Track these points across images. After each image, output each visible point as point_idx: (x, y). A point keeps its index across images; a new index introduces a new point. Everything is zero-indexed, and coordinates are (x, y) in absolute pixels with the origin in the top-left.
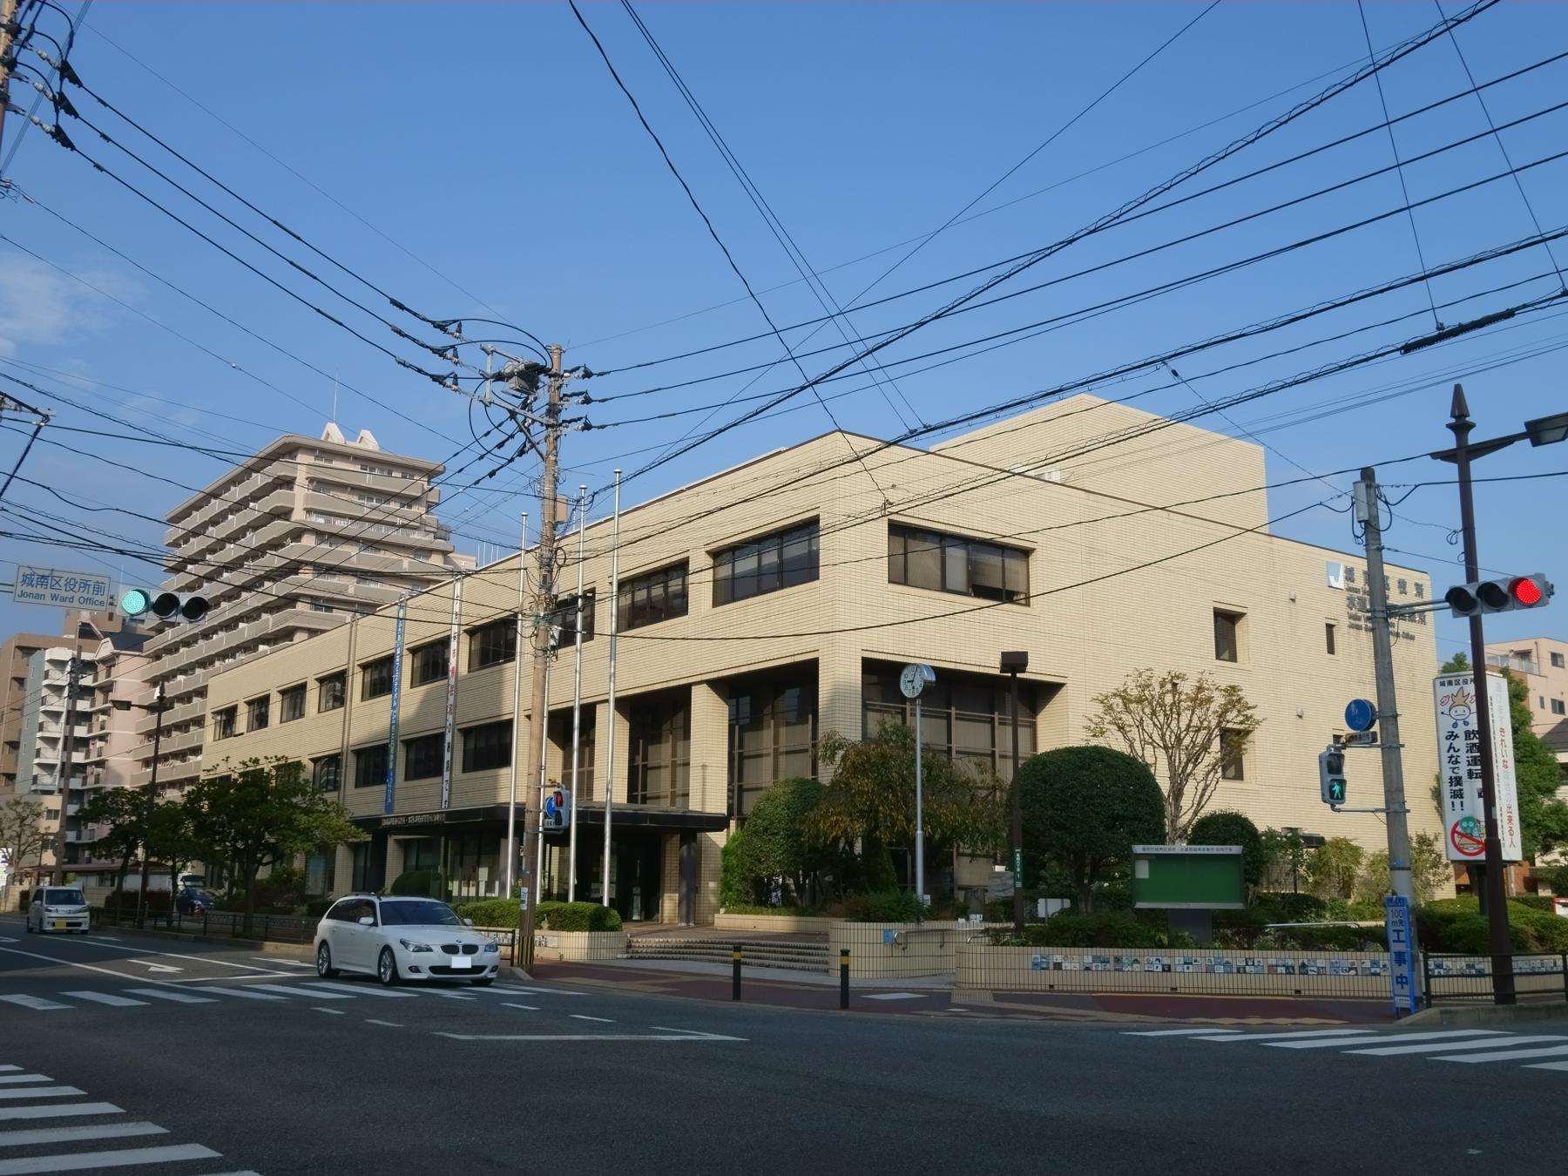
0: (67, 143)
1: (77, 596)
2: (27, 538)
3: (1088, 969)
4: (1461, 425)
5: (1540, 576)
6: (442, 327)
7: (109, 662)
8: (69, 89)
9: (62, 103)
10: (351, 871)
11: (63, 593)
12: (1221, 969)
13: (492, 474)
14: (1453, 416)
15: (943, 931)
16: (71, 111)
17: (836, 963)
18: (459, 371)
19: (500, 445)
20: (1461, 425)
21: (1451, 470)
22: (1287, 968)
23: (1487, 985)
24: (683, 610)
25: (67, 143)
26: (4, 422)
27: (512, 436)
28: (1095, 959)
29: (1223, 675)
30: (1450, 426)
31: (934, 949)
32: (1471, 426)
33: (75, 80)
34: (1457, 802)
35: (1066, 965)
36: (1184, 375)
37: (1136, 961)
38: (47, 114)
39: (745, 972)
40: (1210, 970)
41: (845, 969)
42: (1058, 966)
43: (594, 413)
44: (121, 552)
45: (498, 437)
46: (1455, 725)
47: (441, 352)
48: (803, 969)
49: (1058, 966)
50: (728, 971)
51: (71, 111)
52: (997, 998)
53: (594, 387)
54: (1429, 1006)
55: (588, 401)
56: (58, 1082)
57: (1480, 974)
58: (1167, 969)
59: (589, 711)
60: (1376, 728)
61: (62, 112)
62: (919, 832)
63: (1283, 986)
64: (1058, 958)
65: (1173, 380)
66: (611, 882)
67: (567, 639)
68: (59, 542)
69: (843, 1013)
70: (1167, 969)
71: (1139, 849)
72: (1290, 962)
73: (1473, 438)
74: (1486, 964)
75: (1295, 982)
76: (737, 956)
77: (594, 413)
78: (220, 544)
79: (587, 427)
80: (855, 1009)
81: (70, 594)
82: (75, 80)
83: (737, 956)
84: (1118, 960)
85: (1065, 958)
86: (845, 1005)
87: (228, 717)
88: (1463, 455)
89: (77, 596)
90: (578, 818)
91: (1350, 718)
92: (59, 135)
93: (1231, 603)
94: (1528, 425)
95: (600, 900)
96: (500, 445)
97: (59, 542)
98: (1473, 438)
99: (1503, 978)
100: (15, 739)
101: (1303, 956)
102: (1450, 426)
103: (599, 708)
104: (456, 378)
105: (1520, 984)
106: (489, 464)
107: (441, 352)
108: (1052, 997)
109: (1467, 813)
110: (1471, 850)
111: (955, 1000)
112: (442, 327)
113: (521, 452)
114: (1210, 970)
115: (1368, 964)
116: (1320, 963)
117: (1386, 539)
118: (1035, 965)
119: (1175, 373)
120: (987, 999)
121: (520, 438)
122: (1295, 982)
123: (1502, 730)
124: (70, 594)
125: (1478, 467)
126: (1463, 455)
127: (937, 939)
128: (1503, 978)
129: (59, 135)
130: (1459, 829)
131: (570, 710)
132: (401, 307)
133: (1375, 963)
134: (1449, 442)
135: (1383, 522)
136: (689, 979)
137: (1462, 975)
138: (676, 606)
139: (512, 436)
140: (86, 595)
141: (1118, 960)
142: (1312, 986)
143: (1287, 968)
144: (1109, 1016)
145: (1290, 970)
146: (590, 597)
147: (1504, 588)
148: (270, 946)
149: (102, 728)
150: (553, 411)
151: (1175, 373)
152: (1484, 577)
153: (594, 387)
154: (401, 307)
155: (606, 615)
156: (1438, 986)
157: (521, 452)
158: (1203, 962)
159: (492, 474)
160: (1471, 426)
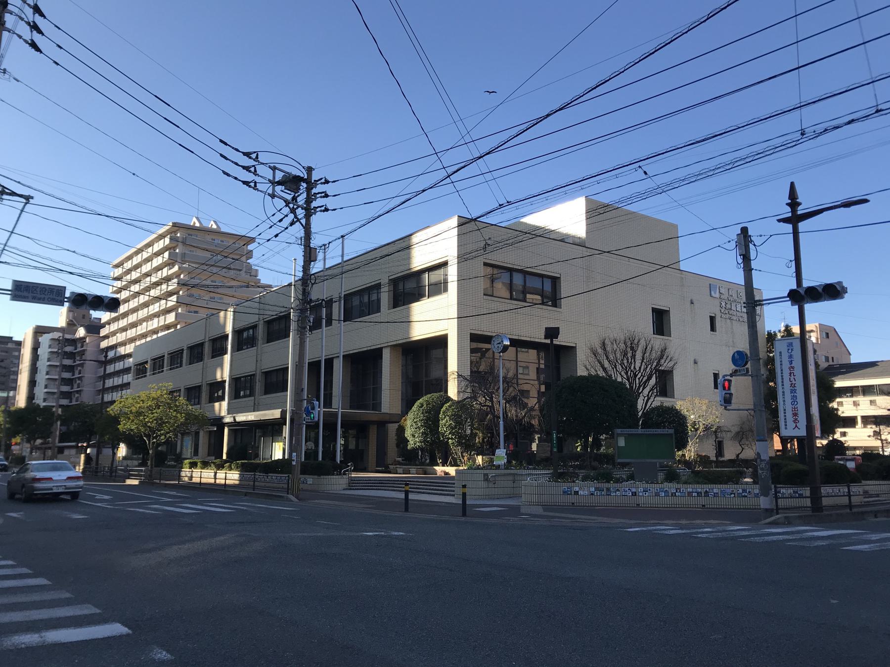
0: (38, 49)
1: (47, 297)
2: (18, 265)
4: (794, 203)
5: (840, 283)
6: (247, 155)
8: (39, 20)
9: (35, 27)
10: (207, 446)
11: (39, 296)
13: (276, 236)
14: (789, 198)
15: (514, 475)
16: (40, 32)
17: (459, 491)
18: (258, 179)
19: (281, 221)
20: (794, 203)
21: (789, 227)
22: (698, 493)
23: (808, 502)
24: (378, 310)
25: (38, 49)
26: (5, 202)
27: (287, 216)
28: (596, 489)
29: (658, 342)
30: (787, 204)
31: (510, 484)
32: (799, 204)
33: (42, 15)
35: (581, 493)
36: (650, 173)
37: (618, 490)
38: (24, 30)
39: (411, 496)
41: (464, 495)
42: (576, 493)
43: (329, 202)
44: (71, 273)
45: (279, 216)
47: (247, 168)
48: (448, 495)
49: (576, 493)
50: (402, 496)
51: (40, 32)
52: (545, 510)
53: (329, 189)
54: (777, 514)
55: (327, 196)
56: (20, 564)
57: (801, 496)
58: (634, 494)
59: (329, 362)
60: (749, 365)
61: (35, 32)
63: (664, 501)
64: (577, 489)
65: (645, 177)
66: (291, 401)
67: (317, 325)
68: (36, 268)
69: (463, 519)
70: (634, 494)
71: (619, 431)
72: (699, 490)
73: (800, 211)
74: (807, 491)
75: (702, 501)
76: (407, 488)
77: (329, 202)
78: (129, 271)
79: (326, 210)
81: (43, 296)
82: (42, 15)
84: (608, 489)
85: (580, 488)
86: (464, 514)
88: (795, 219)
89: (47, 297)
91: (734, 360)
92: (33, 45)
93: (661, 305)
96: (281, 221)
97: (36, 268)
98: (800, 211)
99: (816, 497)
101: (707, 487)
102: (787, 204)
103: (335, 361)
104: (255, 183)
105: (825, 501)
106: (275, 230)
107: (247, 168)
108: (574, 508)
111: (523, 510)
112: (247, 155)
113: (292, 224)
114: (657, 494)
115: (741, 491)
116: (715, 491)
117: (754, 264)
118: (564, 492)
119: (645, 173)
120: (539, 510)
121: (291, 217)
122: (702, 501)
124: (43, 296)
125: (802, 226)
126: (795, 219)
127: (511, 478)
128: (816, 497)
129: (33, 45)
131: (320, 362)
132: (226, 144)
133: (744, 491)
134: (787, 212)
135: (753, 255)
137: (791, 497)
138: (375, 308)
139: (287, 216)
140: (51, 296)
141: (608, 489)
142: (709, 502)
143: (698, 493)
144: (605, 520)
145: (699, 494)
146: (329, 303)
147: (820, 290)
148: (864, 482)
149: (80, 373)
150: (309, 201)
151: (645, 173)
152: (806, 284)
153: (329, 189)
154: (226, 144)
155: (337, 310)
156: (781, 503)
157: (292, 224)
158: (654, 491)
159: (276, 236)
160: (799, 204)
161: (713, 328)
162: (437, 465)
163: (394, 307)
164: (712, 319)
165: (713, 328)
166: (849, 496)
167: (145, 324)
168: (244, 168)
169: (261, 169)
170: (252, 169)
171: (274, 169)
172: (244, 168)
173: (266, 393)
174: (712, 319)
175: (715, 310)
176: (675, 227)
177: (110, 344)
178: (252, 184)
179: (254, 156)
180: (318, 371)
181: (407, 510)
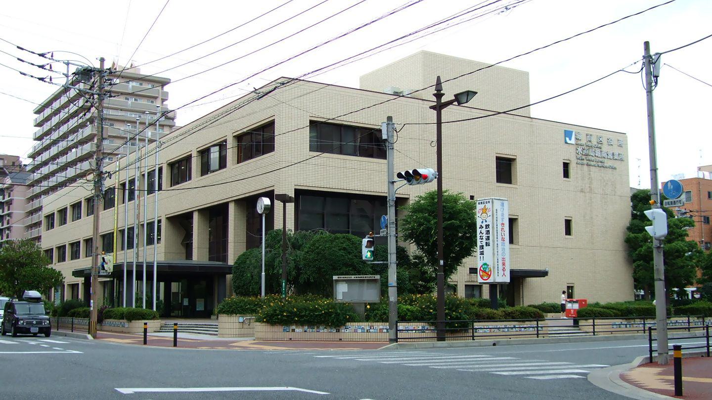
3: (305, 331)
4: (439, 95)
6: (42, 55)
7: (10, 188)
12: (360, 331)
32: (443, 94)
34: (482, 256)
40: (355, 331)
46: (482, 222)
50: (172, 334)
62: (263, 273)
69: (175, 348)
76: (175, 327)
80: (179, 347)
83: (175, 327)
86: (175, 345)
87: (50, 217)
88: (439, 107)
90: (146, 268)
94: (455, 96)
95: (142, 307)
100: (563, 133)
107: (42, 67)
109: (484, 262)
110: (485, 278)
112: (42, 55)
123: (503, 224)
130: (482, 269)
136: (157, 338)
149: (8, 224)
160: (443, 94)
161: (566, 174)
162: (642, 295)
163: (201, 176)
164: (566, 166)
165: (566, 174)
166: (594, 325)
167: (74, 150)
168: (40, 67)
169: (57, 66)
170: (48, 67)
171: (68, 64)
172: (40, 67)
173: (564, 163)
174: (566, 166)
175: (570, 154)
176: (523, 78)
177: (69, 160)
178: (48, 80)
179: (49, 56)
180: (181, 222)
181: (175, 345)
